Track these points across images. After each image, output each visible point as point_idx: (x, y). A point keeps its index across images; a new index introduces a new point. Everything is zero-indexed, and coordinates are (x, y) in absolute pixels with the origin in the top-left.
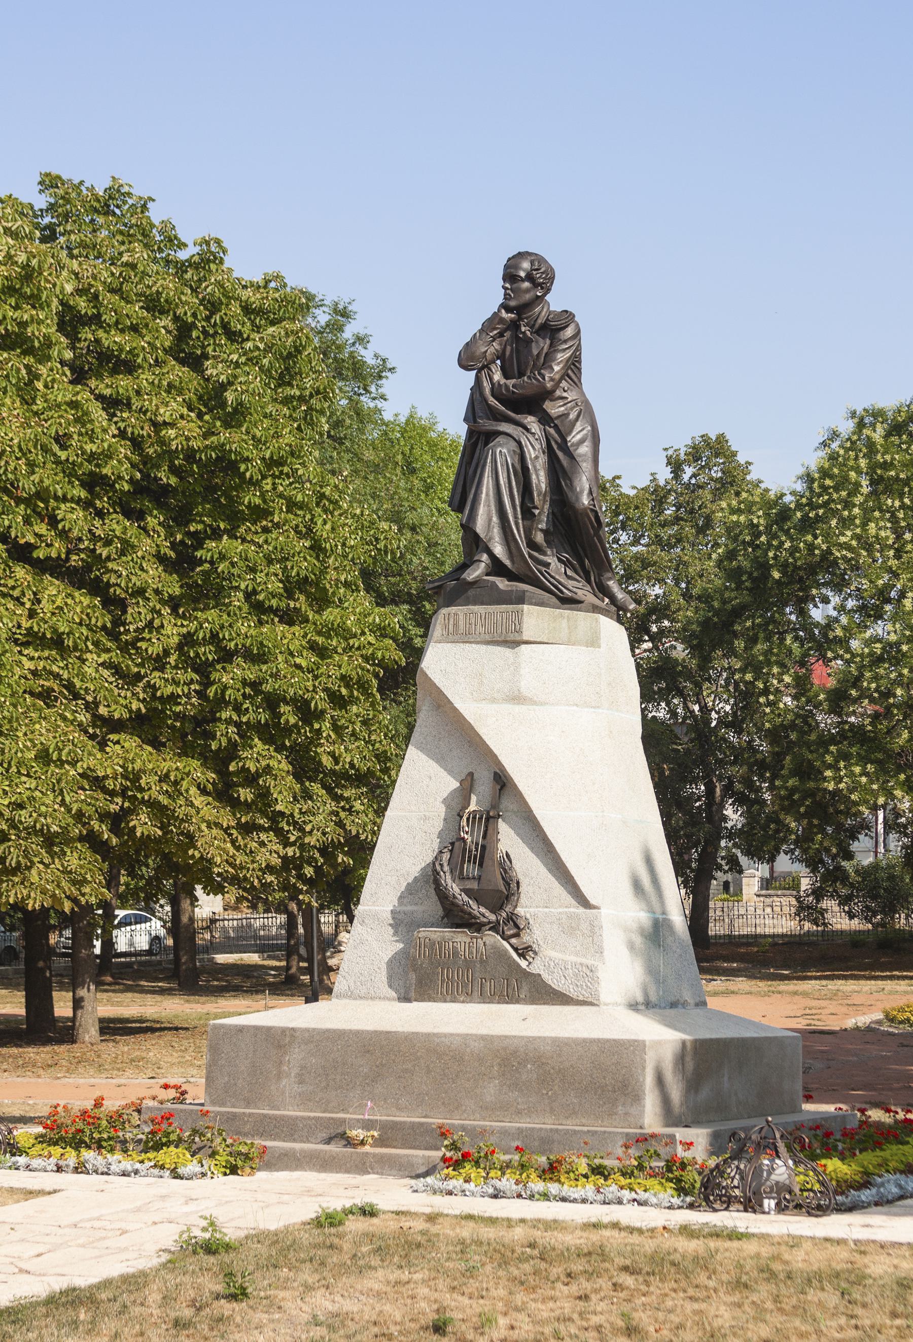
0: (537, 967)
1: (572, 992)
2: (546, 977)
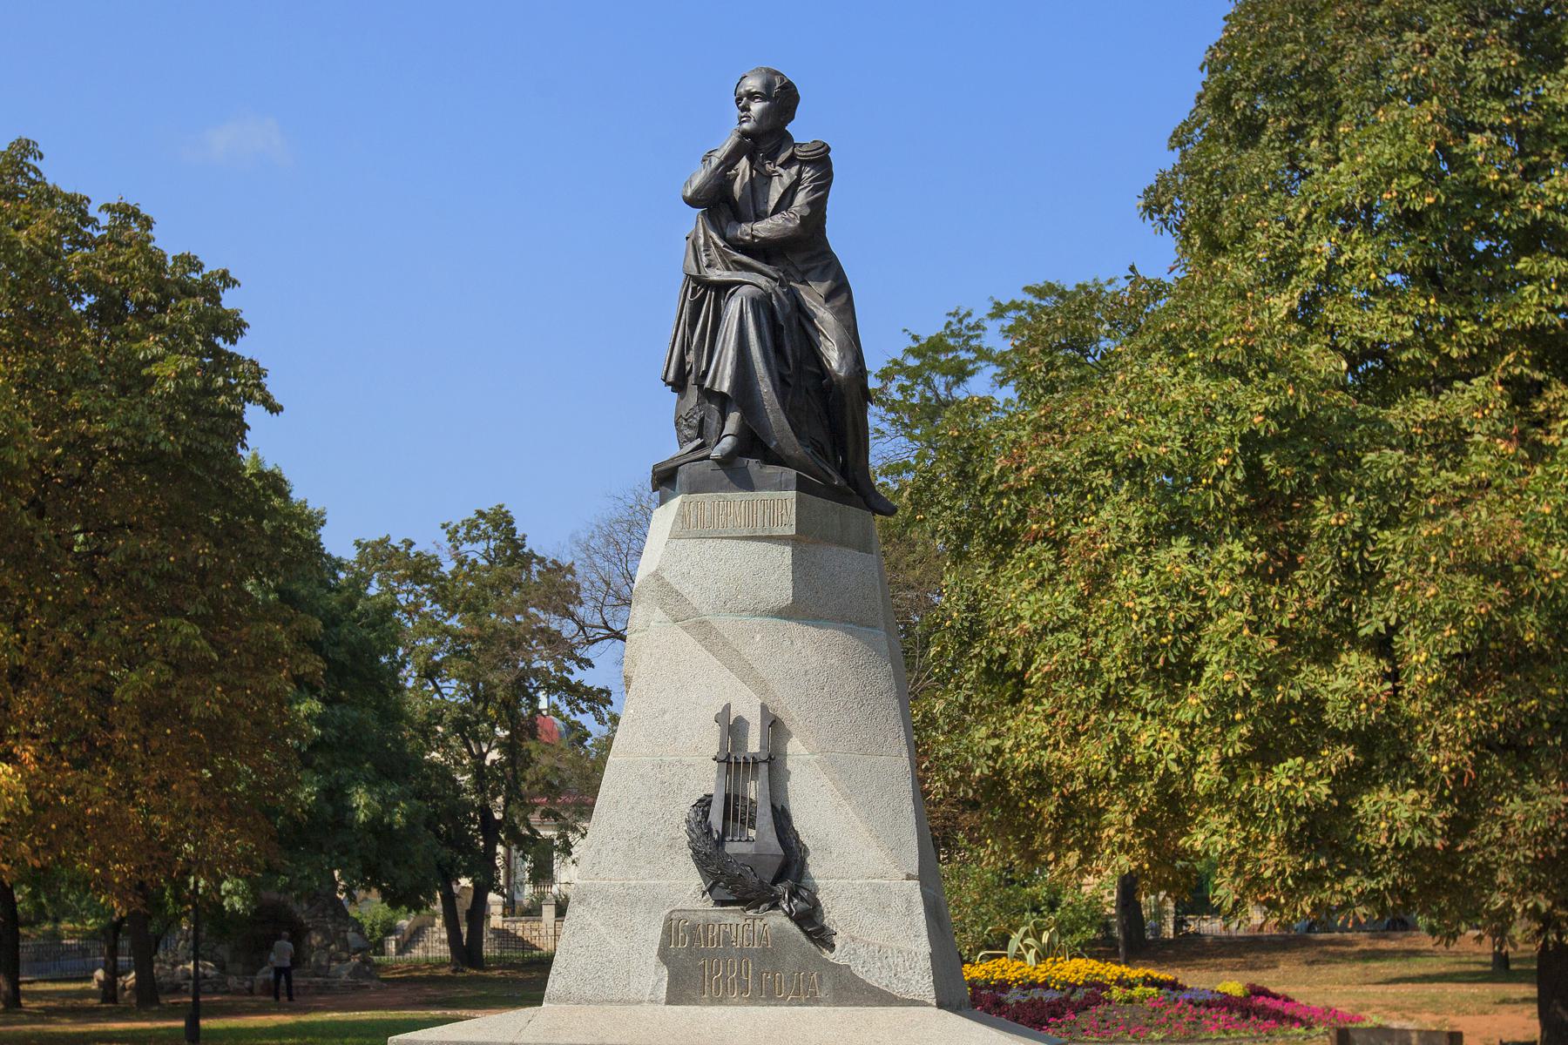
0: (836, 957)
1: (897, 989)
2: (859, 971)
